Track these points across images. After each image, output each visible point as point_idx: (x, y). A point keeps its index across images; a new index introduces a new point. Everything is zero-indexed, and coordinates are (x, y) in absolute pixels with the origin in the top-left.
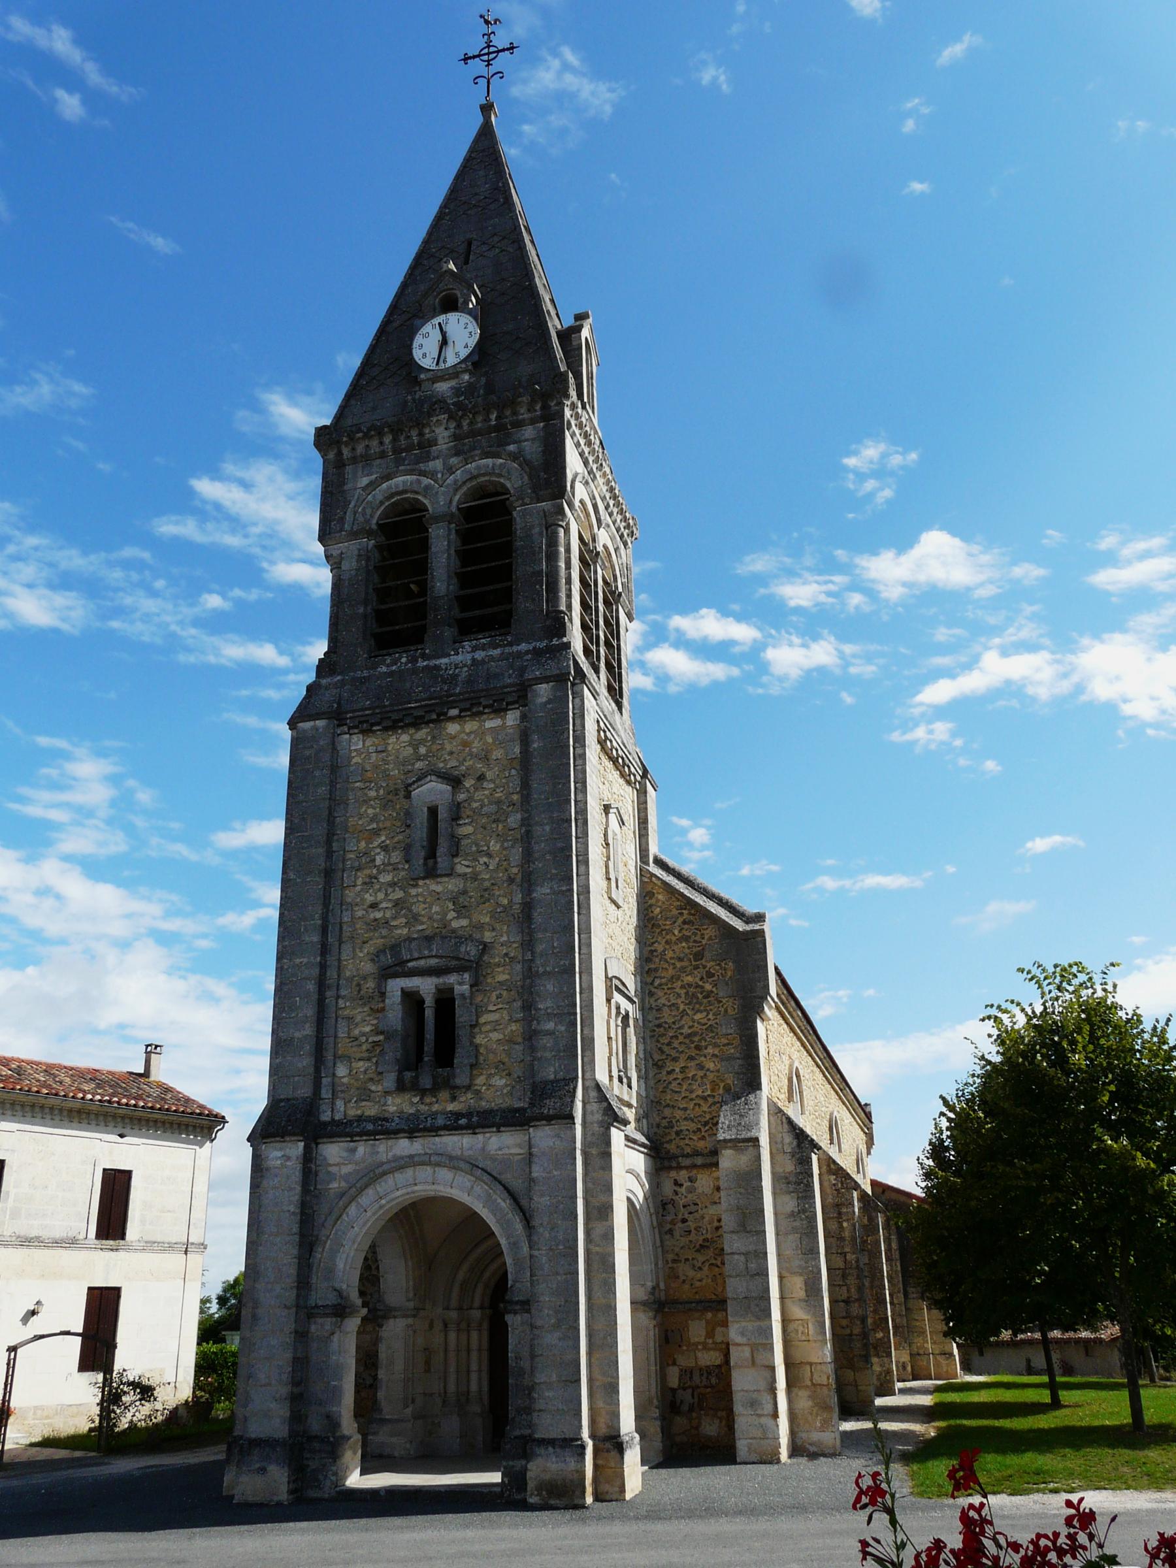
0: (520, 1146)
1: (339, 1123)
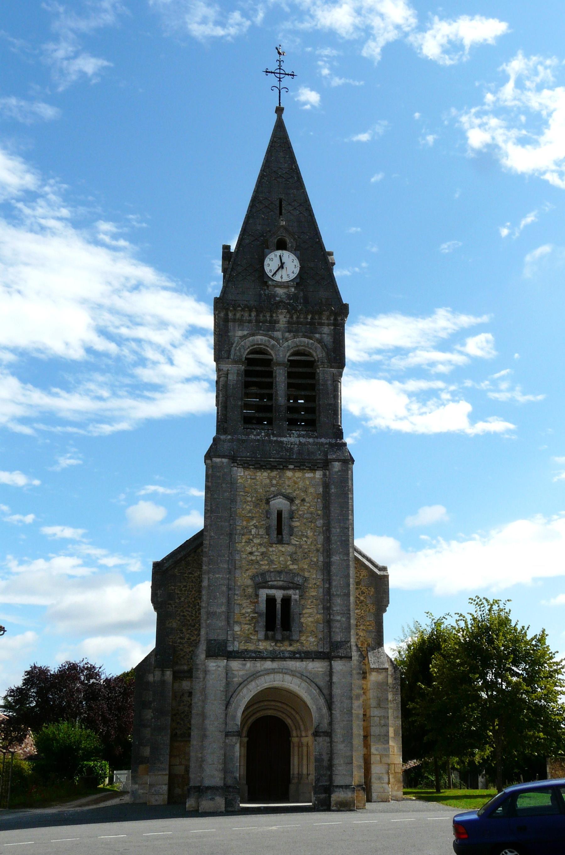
0: (322, 668)
1: (237, 652)
